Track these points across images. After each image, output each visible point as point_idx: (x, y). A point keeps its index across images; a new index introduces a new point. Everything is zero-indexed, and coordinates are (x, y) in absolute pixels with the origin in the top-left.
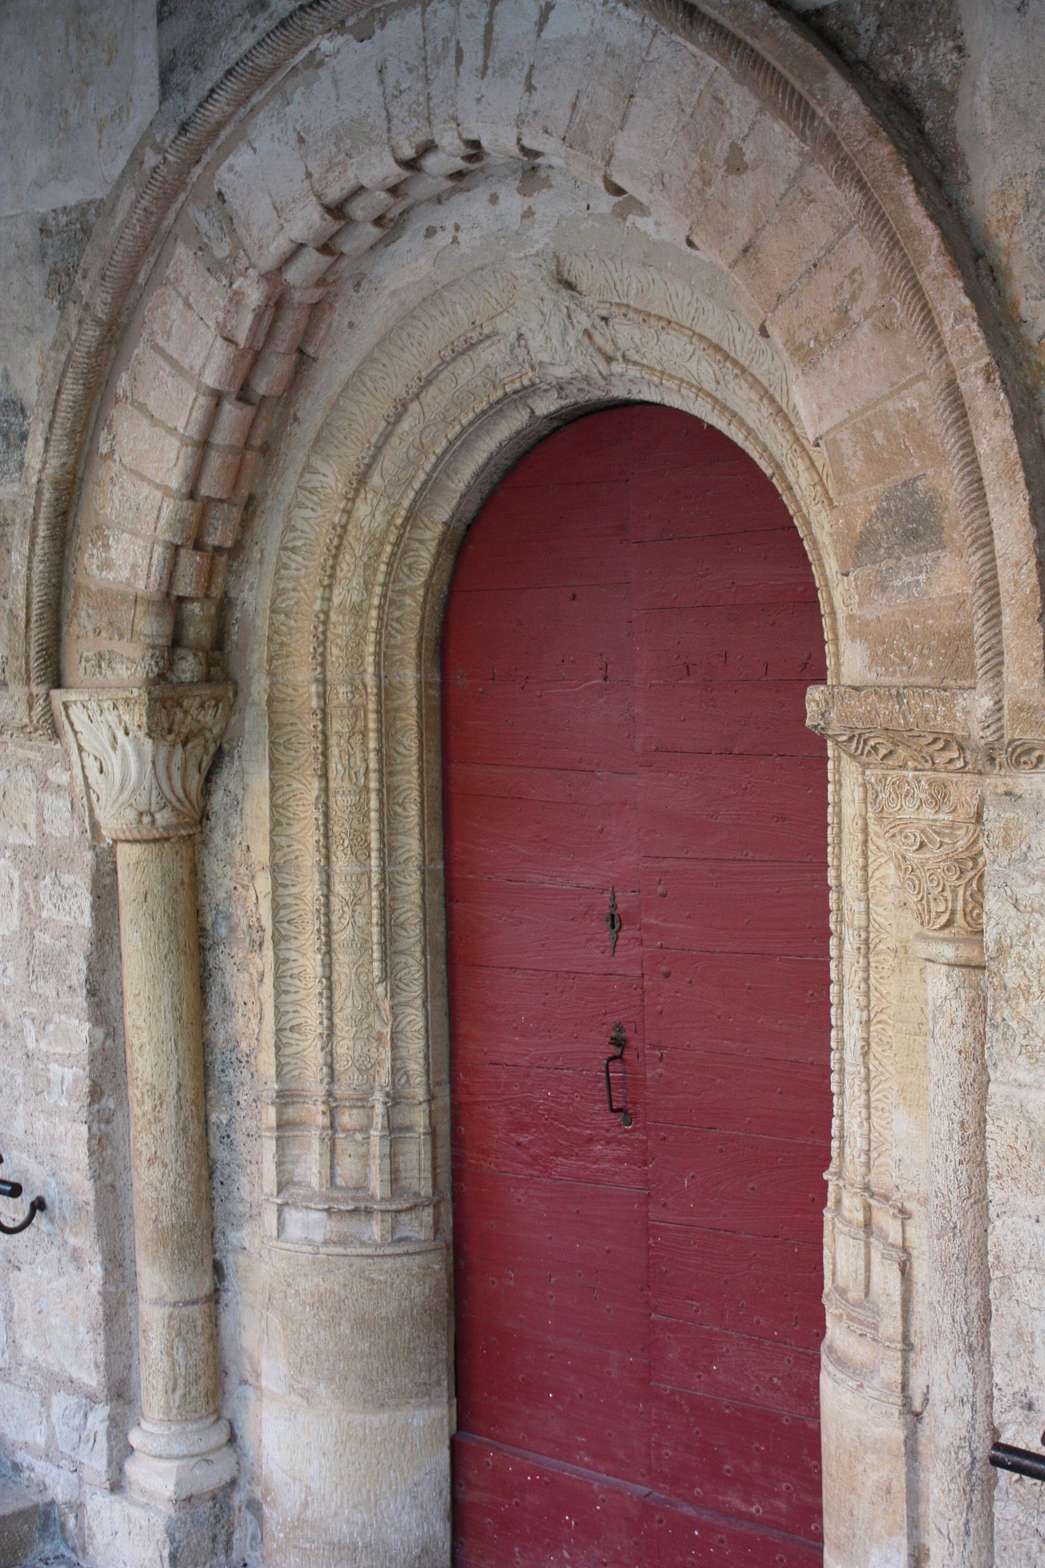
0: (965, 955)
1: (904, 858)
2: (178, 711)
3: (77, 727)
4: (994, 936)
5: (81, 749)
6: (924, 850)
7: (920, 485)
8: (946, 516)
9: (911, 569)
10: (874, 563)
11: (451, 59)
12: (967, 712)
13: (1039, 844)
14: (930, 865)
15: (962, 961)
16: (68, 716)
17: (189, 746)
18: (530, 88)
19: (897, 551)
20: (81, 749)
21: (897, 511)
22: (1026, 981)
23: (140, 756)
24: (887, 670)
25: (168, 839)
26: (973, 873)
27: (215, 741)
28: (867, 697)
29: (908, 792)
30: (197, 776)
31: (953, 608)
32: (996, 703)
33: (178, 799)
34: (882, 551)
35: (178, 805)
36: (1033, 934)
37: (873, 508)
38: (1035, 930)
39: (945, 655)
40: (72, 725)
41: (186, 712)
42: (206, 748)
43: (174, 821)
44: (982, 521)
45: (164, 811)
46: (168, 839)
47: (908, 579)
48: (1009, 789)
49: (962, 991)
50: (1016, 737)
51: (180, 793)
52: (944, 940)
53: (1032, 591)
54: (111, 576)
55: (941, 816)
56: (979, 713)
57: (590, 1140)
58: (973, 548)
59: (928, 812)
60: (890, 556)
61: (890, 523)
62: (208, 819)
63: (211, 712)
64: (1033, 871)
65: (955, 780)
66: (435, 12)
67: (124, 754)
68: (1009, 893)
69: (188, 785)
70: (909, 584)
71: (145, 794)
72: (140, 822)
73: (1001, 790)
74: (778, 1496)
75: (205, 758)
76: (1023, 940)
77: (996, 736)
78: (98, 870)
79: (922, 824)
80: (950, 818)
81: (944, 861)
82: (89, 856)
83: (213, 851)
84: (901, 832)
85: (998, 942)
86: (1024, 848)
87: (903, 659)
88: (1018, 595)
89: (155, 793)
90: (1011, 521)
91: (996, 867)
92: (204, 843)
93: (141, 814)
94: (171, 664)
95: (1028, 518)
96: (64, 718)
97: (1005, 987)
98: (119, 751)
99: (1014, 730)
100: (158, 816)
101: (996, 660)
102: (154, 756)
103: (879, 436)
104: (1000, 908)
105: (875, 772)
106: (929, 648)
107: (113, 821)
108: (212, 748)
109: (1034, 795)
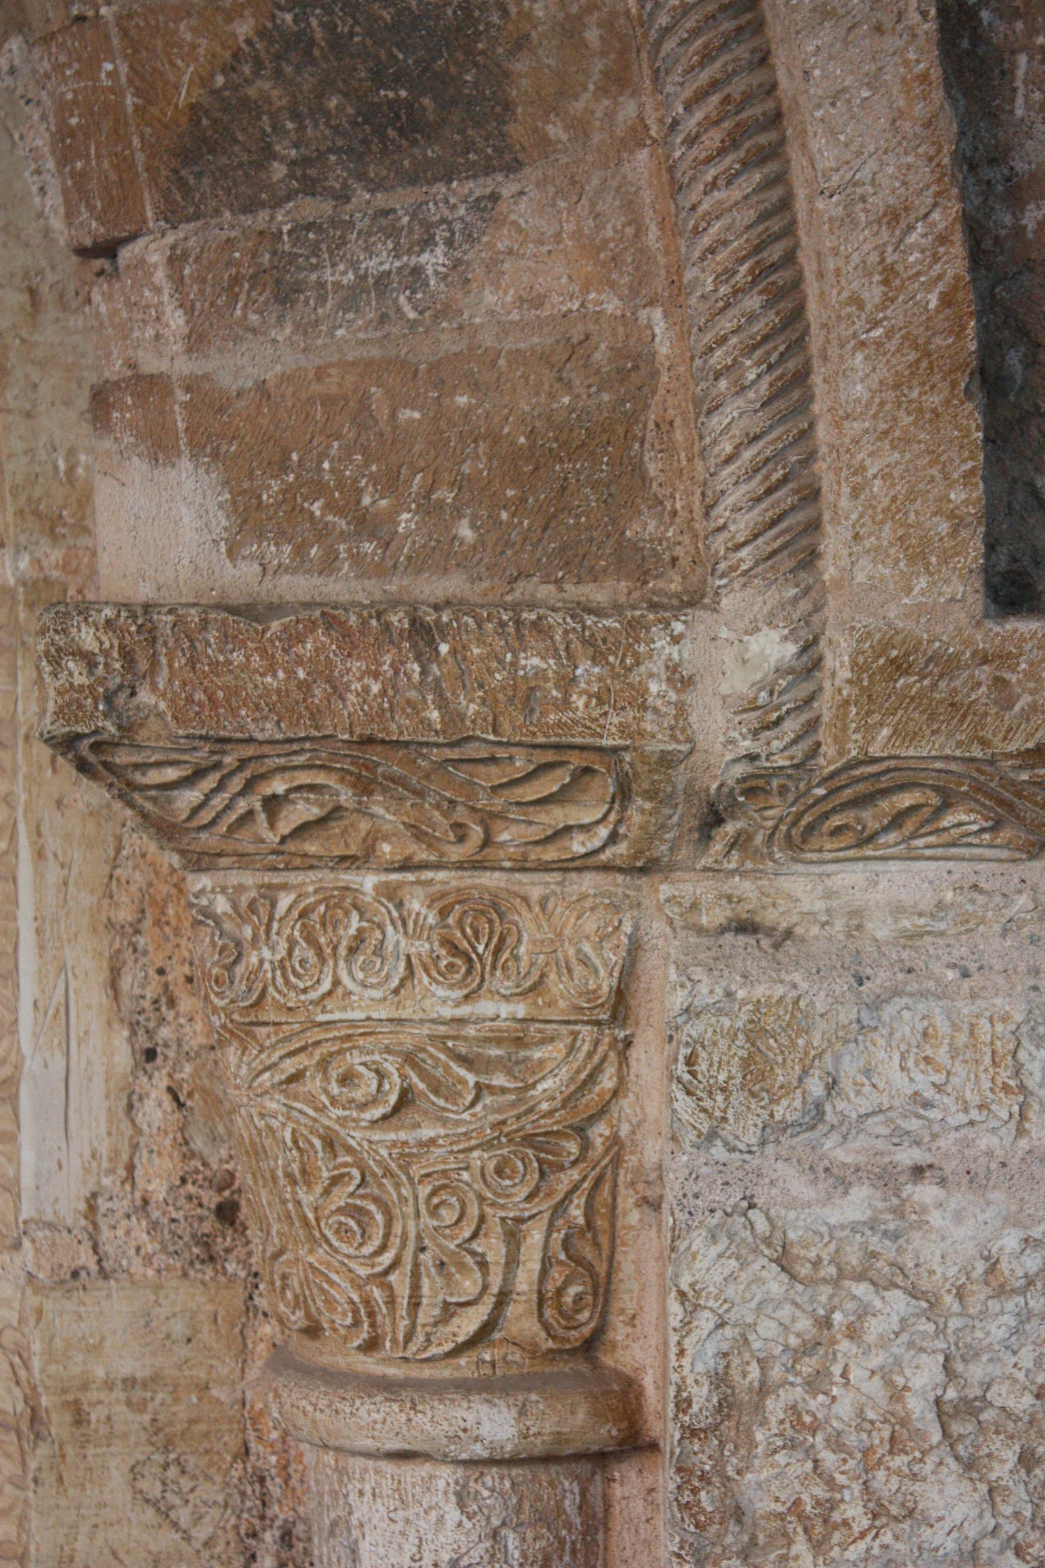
0: (549, 1427)
1: (330, 1143)
4: (708, 1362)
6: (409, 1115)
8: (520, 66)
9: (393, 232)
10: (246, 210)
12: (681, 680)
13: (867, 1072)
14: (437, 1159)
15: (539, 1447)
19: (336, 176)
21: (337, 43)
22: (820, 1491)
24: (300, 551)
26: (575, 1175)
28: (293, 638)
29: (360, 938)
31: (544, 358)
32: (804, 649)
34: (279, 171)
36: (845, 1346)
37: (243, 29)
38: (853, 1333)
39: (519, 506)
44: (756, 79)
47: (380, 261)
48: (742, 911)
49: (512, 1541)
50: (874, 750)
52: (466, 1388)
53: (946, 301)
55: (486, 1007)
56: (738, 683)
58: (729, 160)
59: (440, 1000)
60: (310, 188)
61: (308, 80)
64: (842, 1155)
65: (535, 893)
68: (762, 1226)
70: (382, 281)
73: (713, 916)
76: (808, 1366)
77: (799, 751)
79: (407, 1039)
80: (521, 1010)
81: (487, 1145)
84: (324, 1065)
85: (720, 1379)
86: (816, 1087)
87: (364, 524)
88: (896, 315)
90: (873, 82)
91: (719, 1152)
95: (936, 73)
97: (738, 1514)
99: (869, 730)
101: (799, 517)
104: (731, 1278)
105: (234, 878)
106: (458, 484)
109: (839, 925)
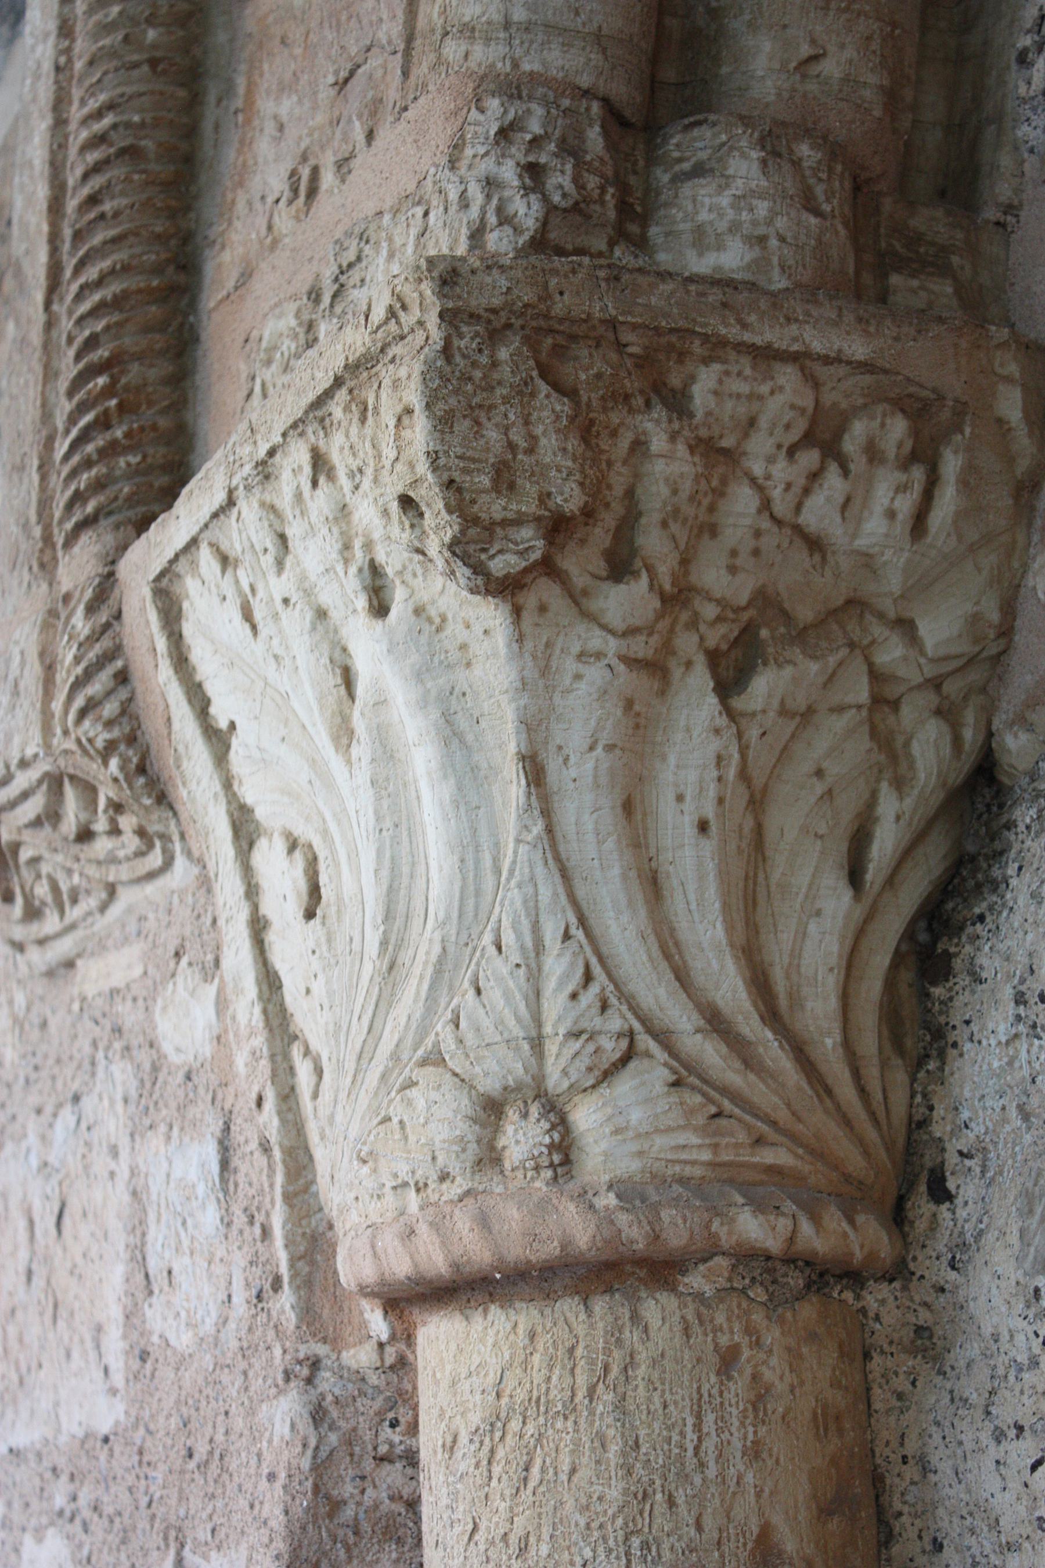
2: (655, 428)
3: (221, 713)
5: (245, 829)
16: (181, 661)
17: (763, 688)
20: (245, 829)
23: (454, 734)
25: (660, 1269)
27: (947, 713)
30: (837, 903)
33: (715, 1022)
35: (710, 1053)
40: (200, 702)
41: (717, 456)
42: (891, 755)
43: (688, 1147)
45: (625, 1085)
46: (660, 1269)
51: (730, 989)
62: (940, 1193)
63: (889, 495)
67: (387, 753)
69: (777, 954)
71: (501, 974)
72: (489, 1158)
75: (888, 806)
78: (325, 1502)
82: (283, 1415)
83: (973, 1389)
89: (559, 967)
92: (927, 1344)
93: (492, 1110)
94: (634, 216)
96: (165, 674)
98: (361, 750)
100: (586, 1117)
102: (534, 727)
107: (387, 1186)
108: (931, 753)
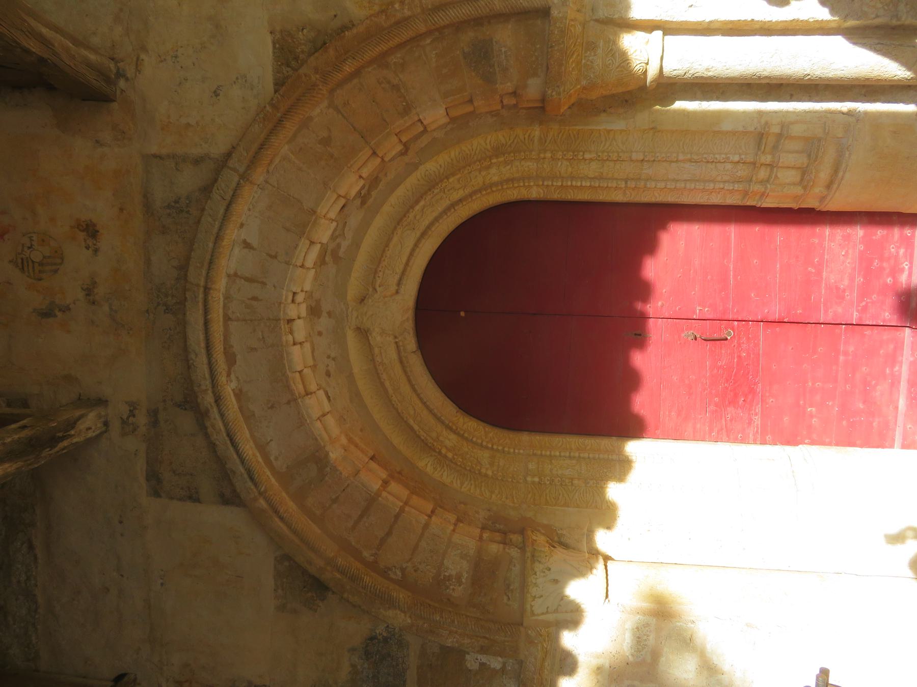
7: (466, 50)
11: (254, 303)
18: (275, 257)
37: (473, 74)
54: (465, 575)
57: (739, 357)
66: (233, 312)
74: (898, 253)
103: (445, 71)
